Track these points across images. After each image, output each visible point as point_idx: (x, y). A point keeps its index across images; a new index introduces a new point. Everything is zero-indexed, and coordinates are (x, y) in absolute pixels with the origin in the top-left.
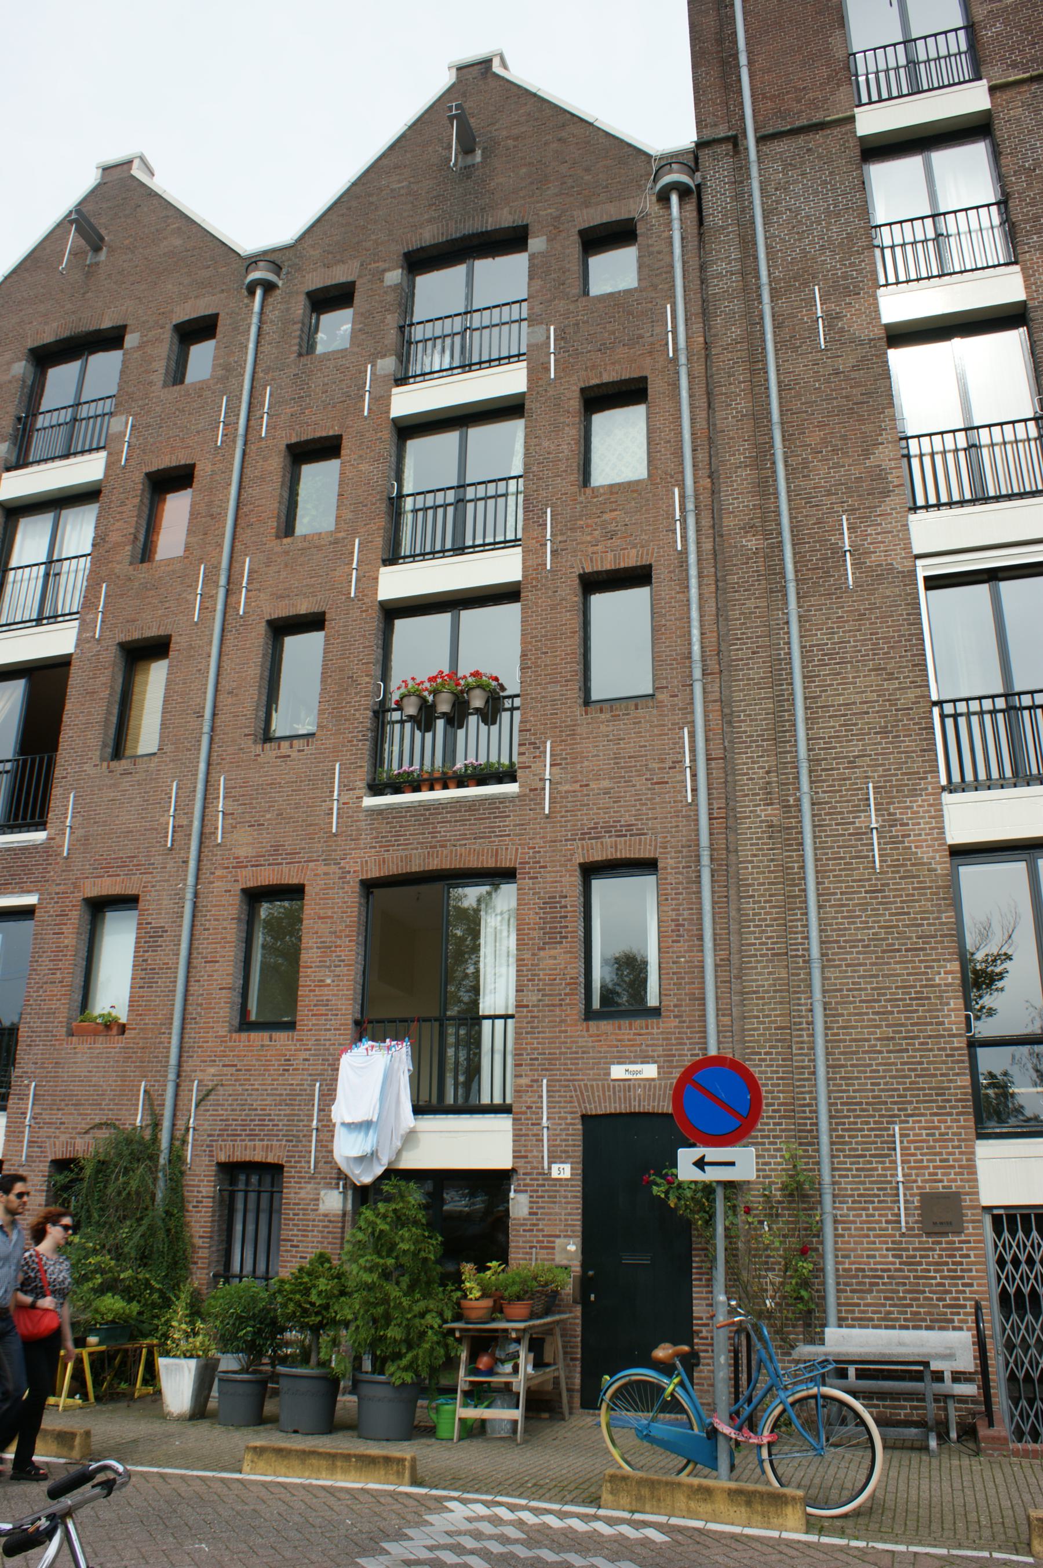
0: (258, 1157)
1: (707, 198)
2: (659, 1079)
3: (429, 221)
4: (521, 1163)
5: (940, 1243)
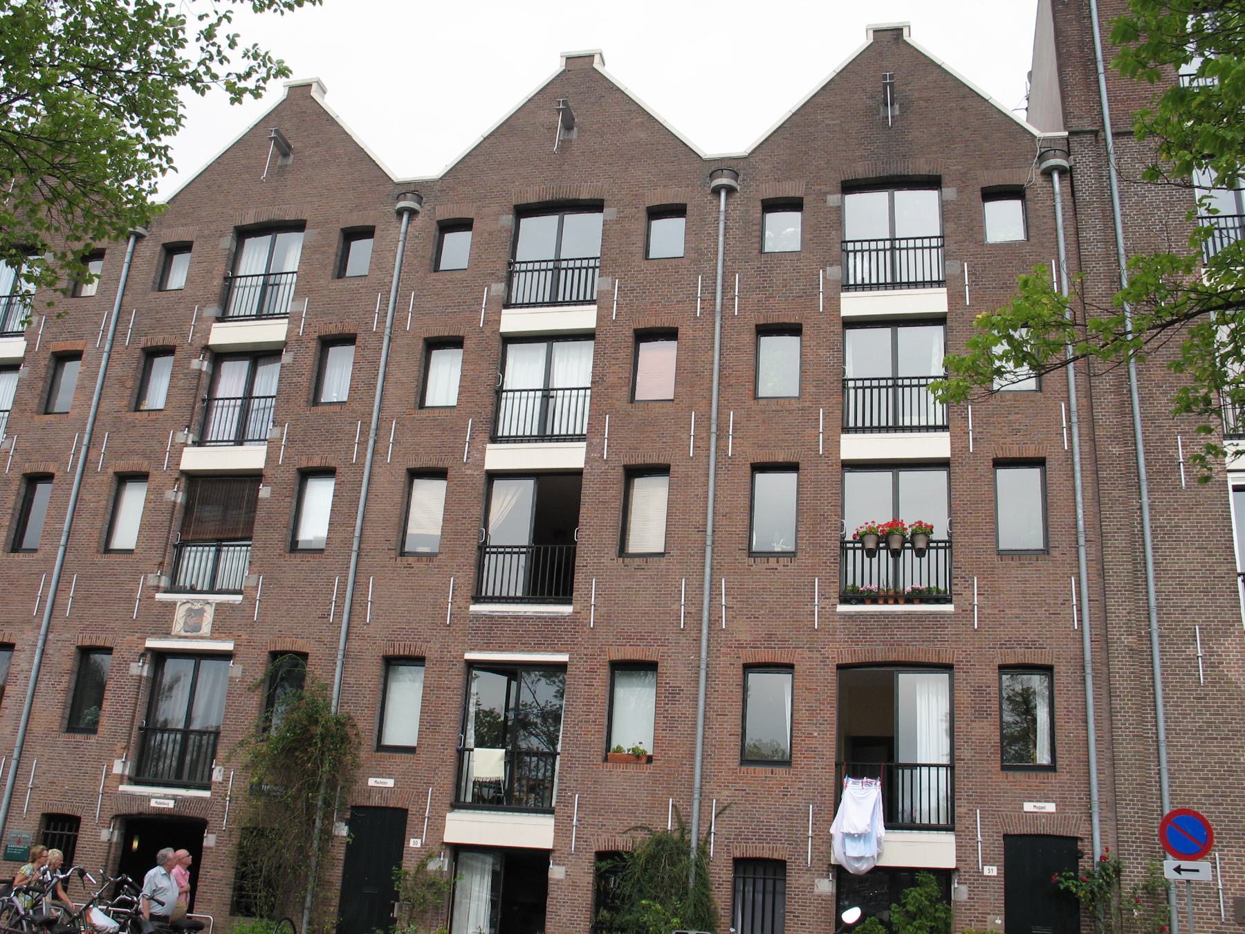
0: (766, 854)
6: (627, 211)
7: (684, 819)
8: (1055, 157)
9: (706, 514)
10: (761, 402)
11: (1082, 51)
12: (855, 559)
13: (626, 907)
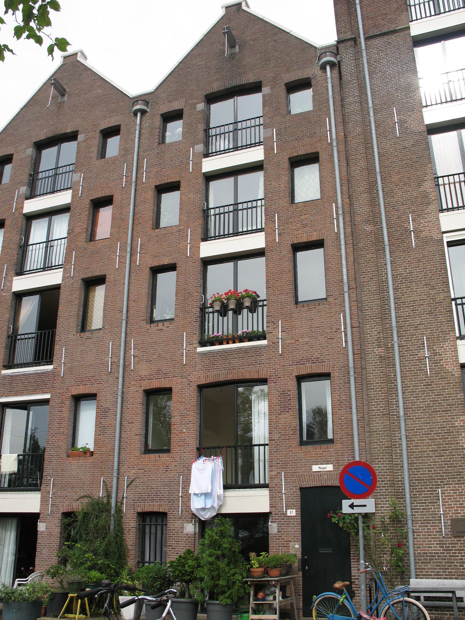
0: (156, 509)
1: (343, 67)
6: (90, 135)
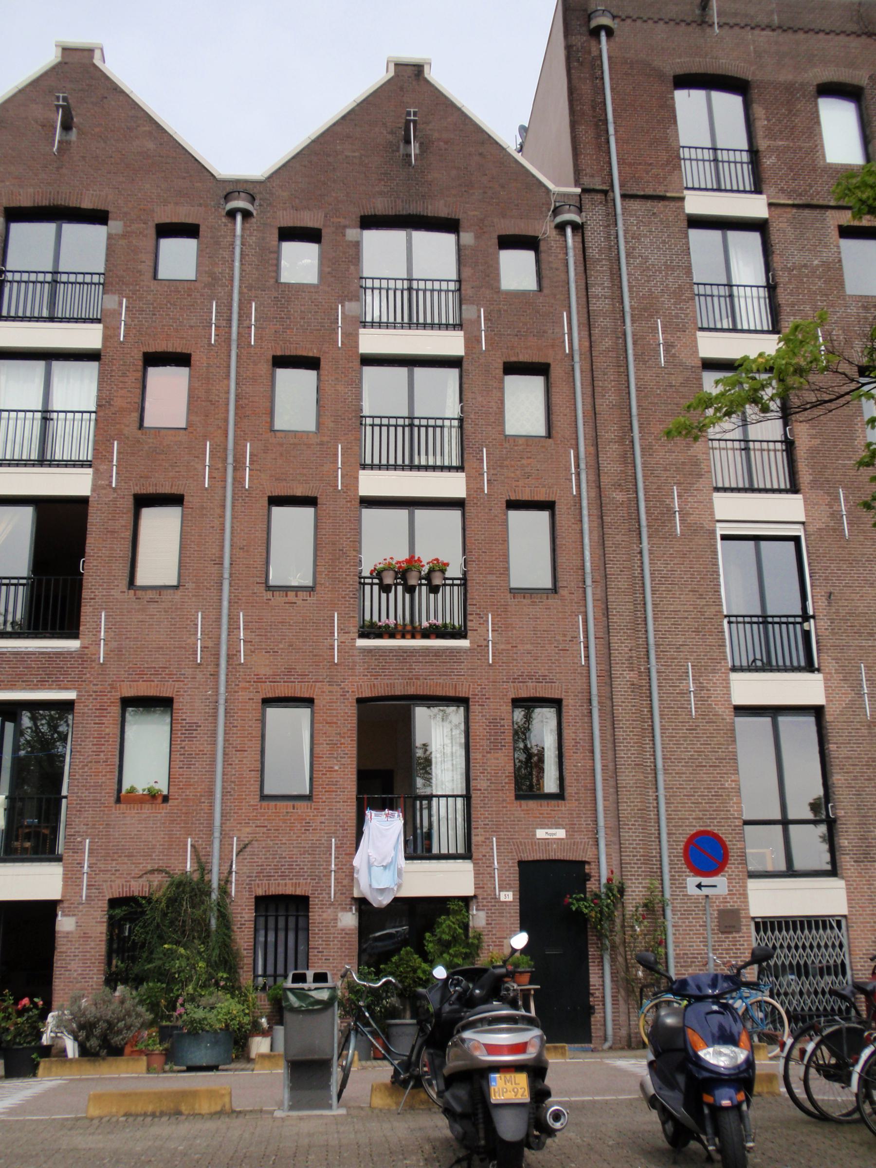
0: (289, 891)
1: (588, 234)
2: (567, 838)
3: (381, 193)
4: (480, 891)
5: (728, 938)
6: (135, 227)
7: (203, 860)
8: (569, 211)
9: (222, 547)
10: (278, 434)
11: (594, 111)
12: (371, 593)
13: (144, 955)
